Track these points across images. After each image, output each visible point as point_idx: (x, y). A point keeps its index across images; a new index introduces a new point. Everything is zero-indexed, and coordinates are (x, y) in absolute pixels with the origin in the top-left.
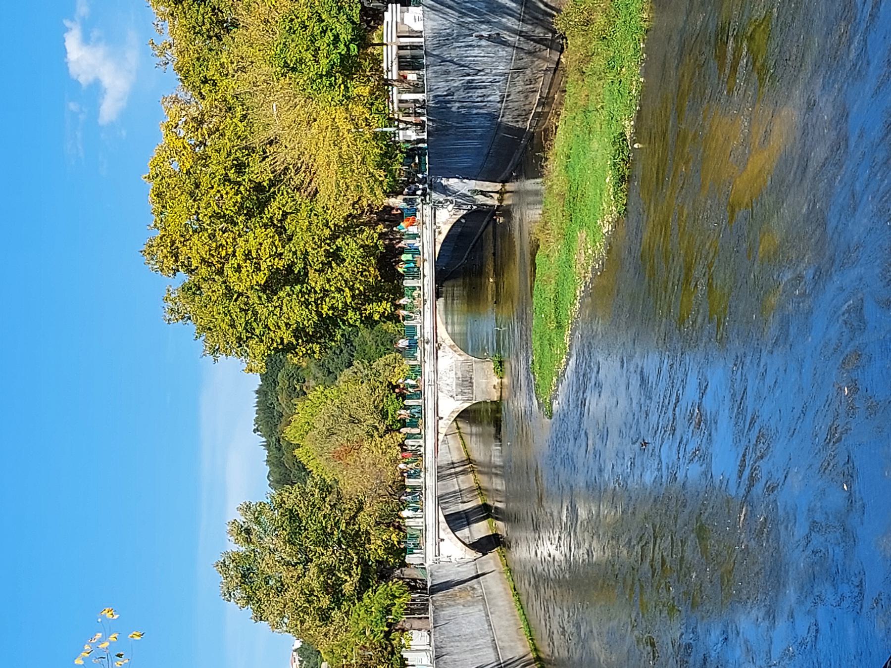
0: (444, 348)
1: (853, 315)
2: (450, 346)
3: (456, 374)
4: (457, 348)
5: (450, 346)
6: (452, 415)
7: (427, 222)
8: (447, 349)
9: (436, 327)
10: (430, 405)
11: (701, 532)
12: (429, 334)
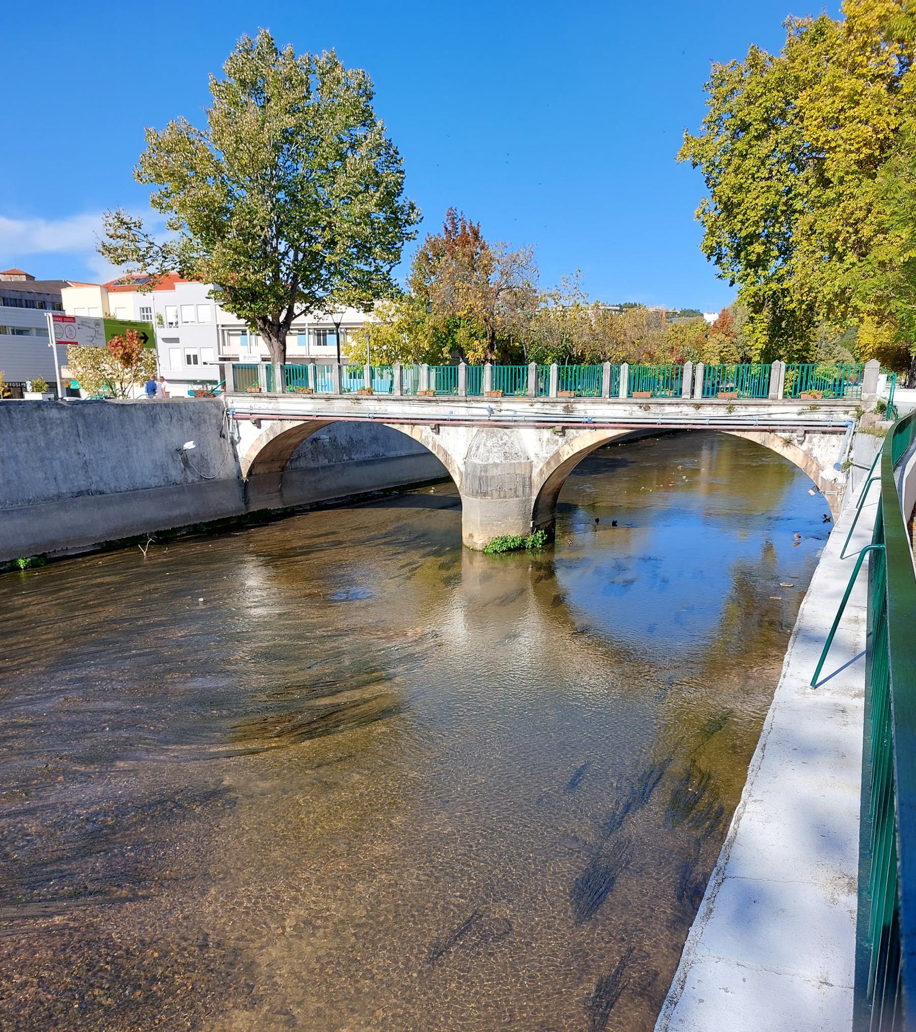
0: (556, 442)
1: (290, 280)
2: (557, 454)
3: (496, 465)
4: (554, 466)
5: (557, 454)
6: (442, 453)
7: (816, 416)
8: (554, 448)
9: (595, 428)
10: (460, 411)
11: (413, 239)
12: (582, 414)
